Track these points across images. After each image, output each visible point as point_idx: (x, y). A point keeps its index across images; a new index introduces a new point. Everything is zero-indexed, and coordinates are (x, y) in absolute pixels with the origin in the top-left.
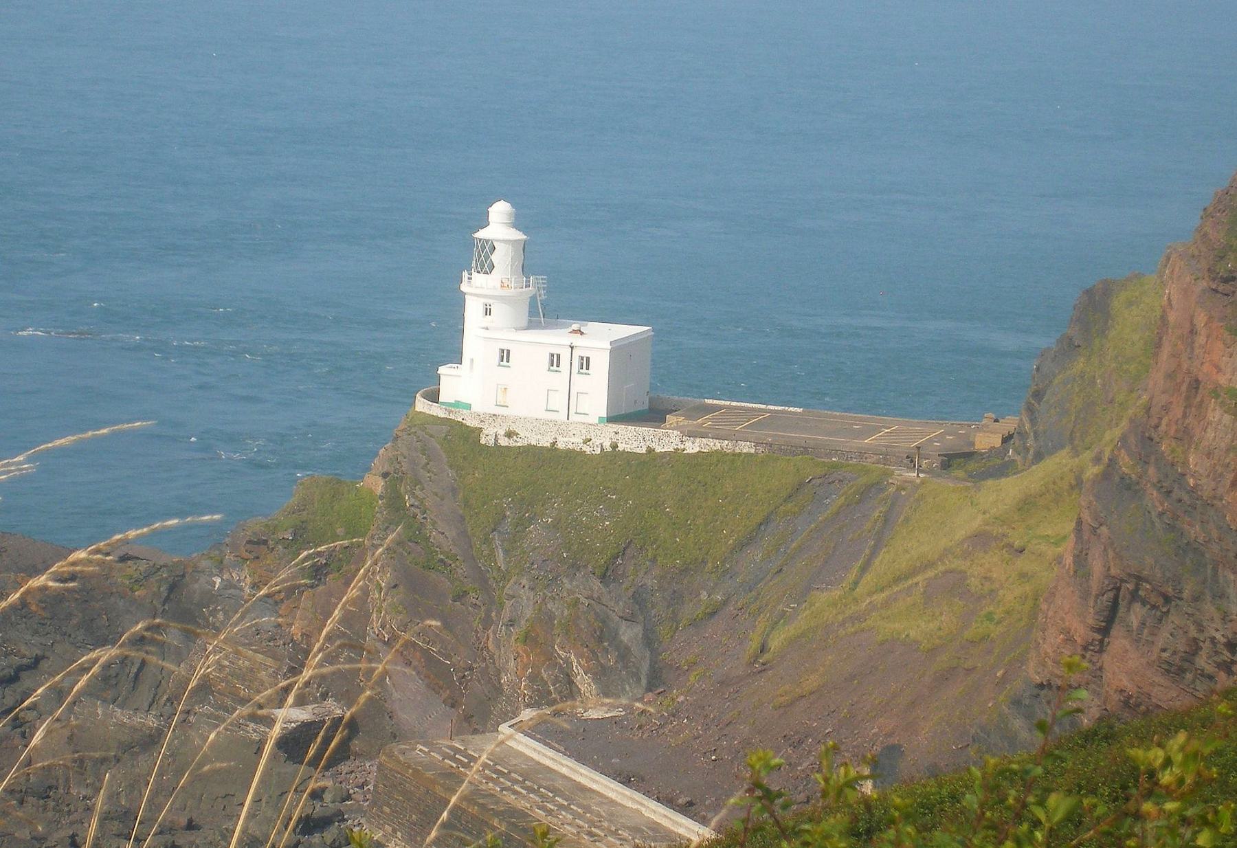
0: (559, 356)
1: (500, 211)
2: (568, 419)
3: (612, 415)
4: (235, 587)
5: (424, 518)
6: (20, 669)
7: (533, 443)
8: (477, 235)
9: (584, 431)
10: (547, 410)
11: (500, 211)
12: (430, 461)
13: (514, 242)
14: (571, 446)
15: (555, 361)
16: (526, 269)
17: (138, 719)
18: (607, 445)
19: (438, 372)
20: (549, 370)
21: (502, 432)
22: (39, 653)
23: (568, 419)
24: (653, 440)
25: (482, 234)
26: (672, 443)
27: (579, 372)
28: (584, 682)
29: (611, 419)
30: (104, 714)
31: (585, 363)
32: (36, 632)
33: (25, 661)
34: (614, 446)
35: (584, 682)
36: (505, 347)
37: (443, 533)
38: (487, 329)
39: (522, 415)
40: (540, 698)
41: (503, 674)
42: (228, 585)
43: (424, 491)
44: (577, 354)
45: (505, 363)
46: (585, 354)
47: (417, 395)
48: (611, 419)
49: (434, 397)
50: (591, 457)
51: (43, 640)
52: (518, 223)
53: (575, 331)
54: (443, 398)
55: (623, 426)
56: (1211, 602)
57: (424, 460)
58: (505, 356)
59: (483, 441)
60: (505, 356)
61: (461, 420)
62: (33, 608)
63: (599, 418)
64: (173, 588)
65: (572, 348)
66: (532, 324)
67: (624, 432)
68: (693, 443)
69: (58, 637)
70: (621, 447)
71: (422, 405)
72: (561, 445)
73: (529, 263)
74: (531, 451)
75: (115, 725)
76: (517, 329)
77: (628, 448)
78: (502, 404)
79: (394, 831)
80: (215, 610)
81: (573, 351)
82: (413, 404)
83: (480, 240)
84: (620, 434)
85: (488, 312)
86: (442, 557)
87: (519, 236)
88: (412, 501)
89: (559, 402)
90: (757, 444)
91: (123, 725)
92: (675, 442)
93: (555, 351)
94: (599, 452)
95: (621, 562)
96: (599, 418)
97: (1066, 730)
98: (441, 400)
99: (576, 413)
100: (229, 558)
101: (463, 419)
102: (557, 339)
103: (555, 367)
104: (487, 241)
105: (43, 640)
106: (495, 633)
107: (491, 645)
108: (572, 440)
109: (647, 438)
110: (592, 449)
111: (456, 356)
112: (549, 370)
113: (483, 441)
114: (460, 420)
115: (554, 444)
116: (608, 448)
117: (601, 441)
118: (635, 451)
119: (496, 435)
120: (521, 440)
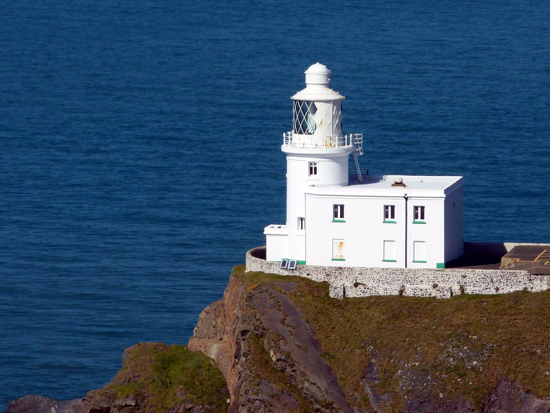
0: (393, 208)
2: (406, 267)
3: (452, 259)
5: (293, 371)
7: (382, 293)
8: (295, 97)
9: (431, 277)
10: (384, 261)
12: (287, 316)
13: (334, 102)
14: (419, 294)
18: (456, 289)
19: (265, 233)
20: (384, 222)
23: (406, 267)
24: (501, 281)
25: (300, 96)
26: (520, 282)
27: (414, 223)
34: (462, 289)
36: (339, 202)
37: (315, 384)
38: (314, 186)
39: (369, 266)
43: (288, 345)
44: (411, 204)
46: (419, 203)
47: (247, 253)
49: (261, 254)
50: (443, 302)
54: (271, 256)
55: (470, 270)
56: (445, 326)
57: (280, 316)
59: (332, 295)
61: (306, 276)
63: (437, 264)
65: (406, 199)
67: (471, 276)
68: (541, 280)
70: (469, 290)
78: (339, 258)
81: (408, 201)
82: (242, 262)
83: (301, 102)
84: (467, 278)
85: (313, 170)
86: (318, 406)
87: (335, 96)
88: (279, 355)
92: (523, 282)
93: (390, 203)
94: (449, 297)
95: (496, 398)
96: (437, 264)
98: (304, 260)
99: (414, 262)
101: (308, 275)
103: (339, 218)
104: (308, 102)
108: (420, 286)
109: (495, 279)
110: (442, 294)
112: (384, 222)
113: (332, 295)
114: (305, 275)
115: (401, 292)
117: (450, 286)
118: (483, 293)
119: (344, 287)
120: (368, 291)
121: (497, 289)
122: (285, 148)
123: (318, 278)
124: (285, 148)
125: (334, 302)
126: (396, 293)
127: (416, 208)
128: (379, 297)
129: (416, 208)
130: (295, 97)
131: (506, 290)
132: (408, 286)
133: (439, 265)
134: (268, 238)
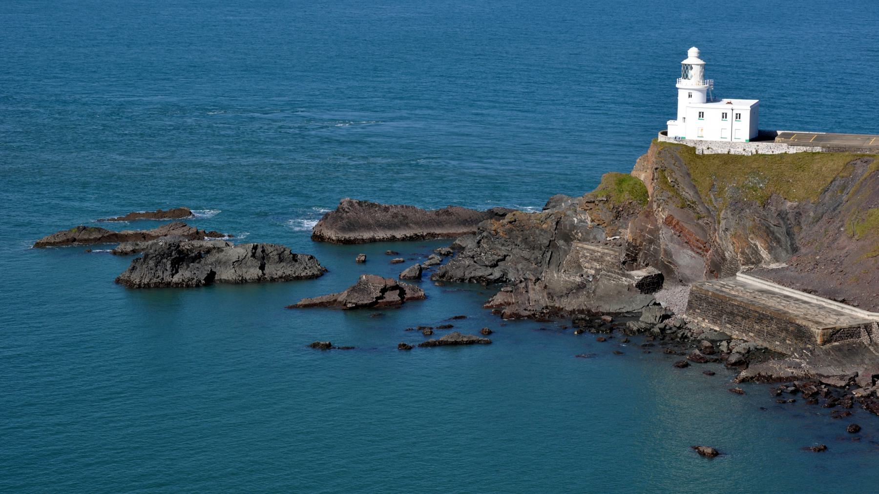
1: (693, 52)
4: (584, 222)
6: (498, 261)
7: (720, 152)
8: (683, 62)
11: (693, 52)
13: (701, 65)
14: (737, 153)
15: (724, 116)
16: (705, 76)
17: (572, 278)
21: (705, 148)
22: (506, 254)
25: (685, 62)
28: (764, 253)
29: (752, 140)
30: (558, 277)
31: (738, 116)
32: (503, 245)
33: (500, 257)
35: (764, 253)
36: (701, 110)
40: (747, 262)
41: (726, 252)
42: (581, 221)
45: (724, 119)
46: (738, 112)
48: (752, 140)
49: (665, 134)
50: (747, 157)
51: (507, 248)
52: (701, 56)
53: (728, 103)
58: (701, 115)
59: (697, 153)
60: (701, 115)
62: (501, 234)
64: (557, 223)
66: (708, 101)
69: (514, 247)
71: (661, 138)
72: (732, 152)
73: (707, 72)
74: (718, 156)
75: (563, 281)
76: (704, 103)
77: (764, 152)
79: (704, 319)
80: (577, 232)
83: (685, 65)
85: (690, 96)
87: (702, 62)
88: (672, 180)
89: (727, 134)
90: (823, 147)
91: (566, 281)
93: (725, 111)
97: (634, 333)
100: (579, 209)
102: (723, 105)
103: (724, 119)
104: (689, 65)
105: (507, 248)
106: (718, 234)
107: (718, 240)
111: (674, 116)
114: (685, 144)
116: (754, 152)
121: (773, 152)
122: (678, 86)
123: (691, 145)
124: (678, 86)
125: (698, 156)
126: (726, 153)
127: (737, 114)
128: (718, 154)
129: (737, 114)
130: (683, 62)
131: (777, 152)
132: (732, 149)
133: (746, 141)
134: (669, 126)
